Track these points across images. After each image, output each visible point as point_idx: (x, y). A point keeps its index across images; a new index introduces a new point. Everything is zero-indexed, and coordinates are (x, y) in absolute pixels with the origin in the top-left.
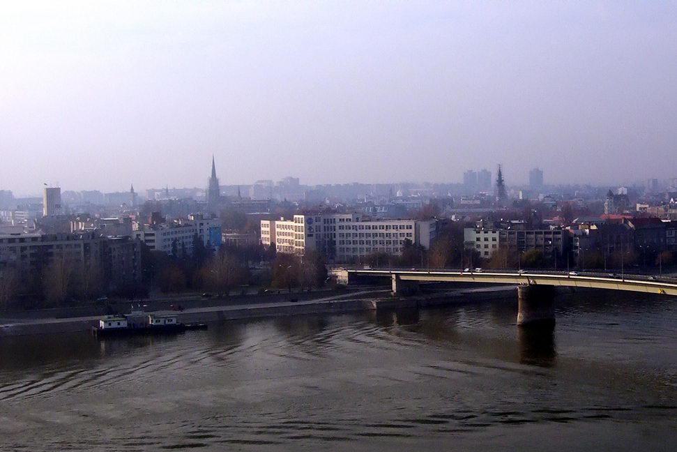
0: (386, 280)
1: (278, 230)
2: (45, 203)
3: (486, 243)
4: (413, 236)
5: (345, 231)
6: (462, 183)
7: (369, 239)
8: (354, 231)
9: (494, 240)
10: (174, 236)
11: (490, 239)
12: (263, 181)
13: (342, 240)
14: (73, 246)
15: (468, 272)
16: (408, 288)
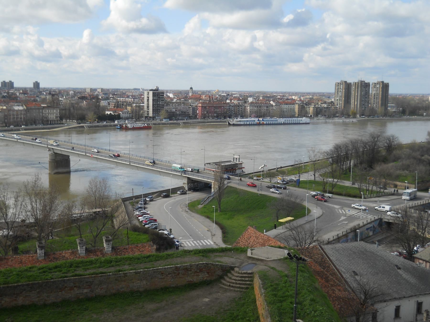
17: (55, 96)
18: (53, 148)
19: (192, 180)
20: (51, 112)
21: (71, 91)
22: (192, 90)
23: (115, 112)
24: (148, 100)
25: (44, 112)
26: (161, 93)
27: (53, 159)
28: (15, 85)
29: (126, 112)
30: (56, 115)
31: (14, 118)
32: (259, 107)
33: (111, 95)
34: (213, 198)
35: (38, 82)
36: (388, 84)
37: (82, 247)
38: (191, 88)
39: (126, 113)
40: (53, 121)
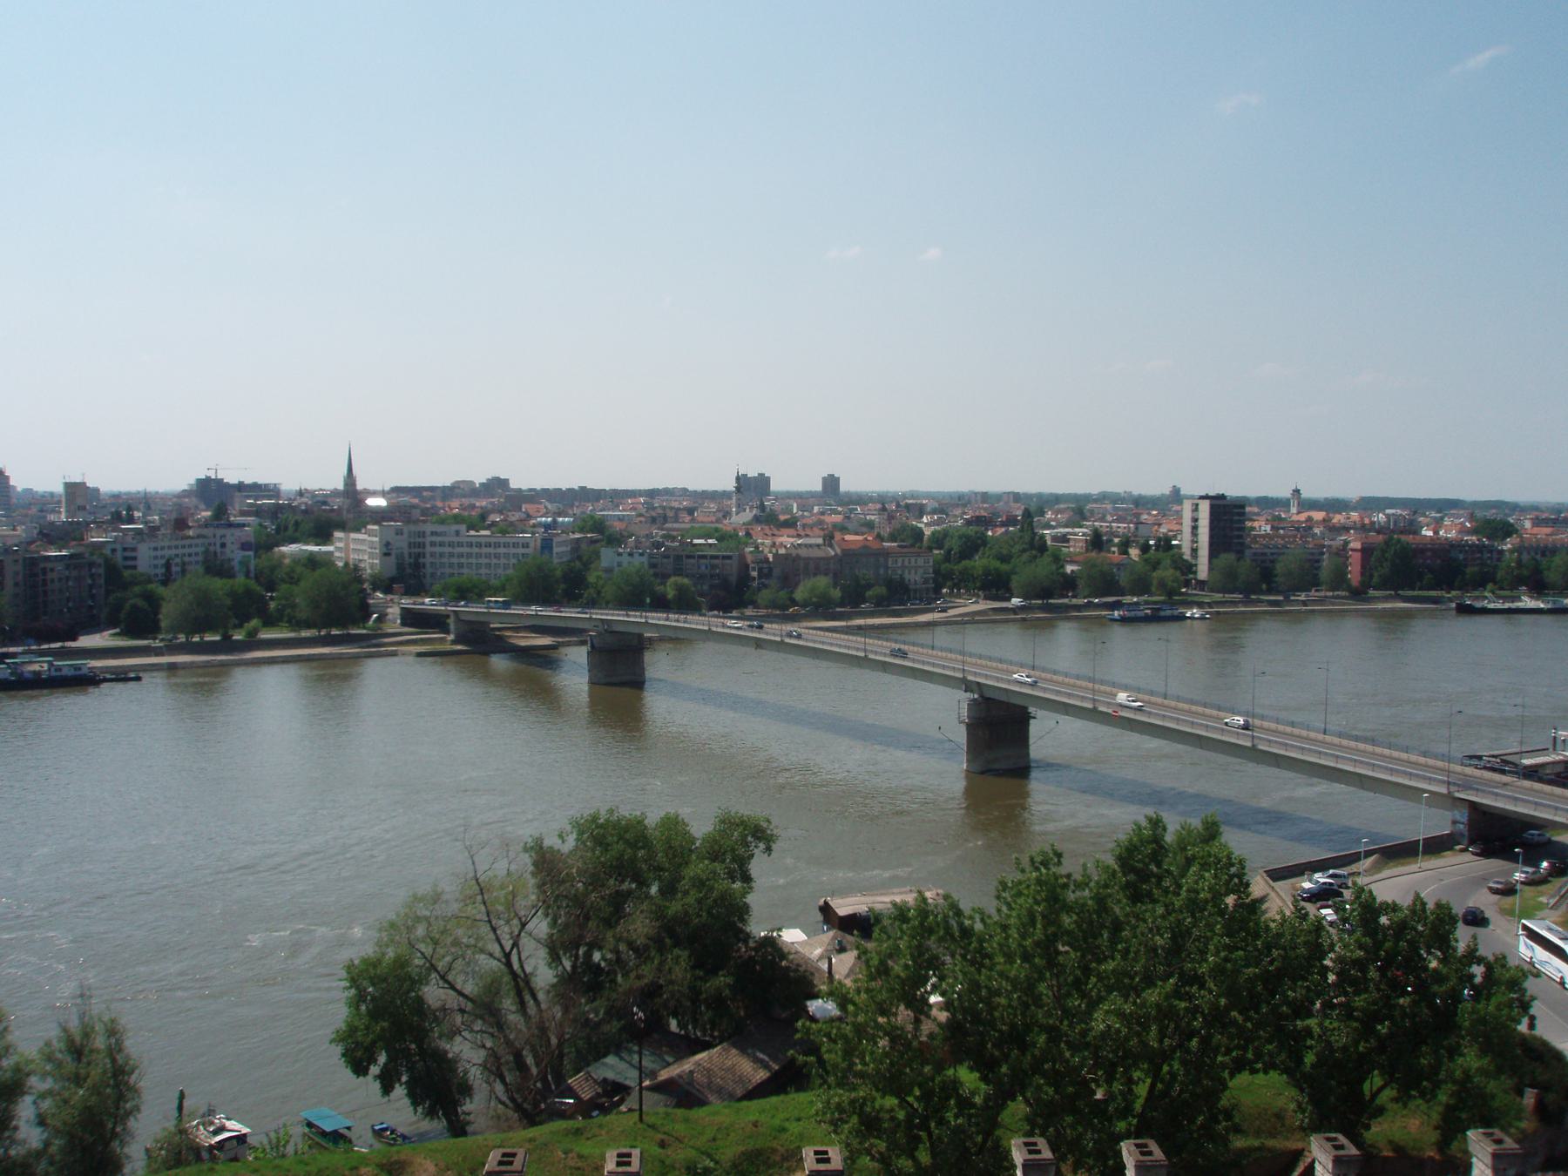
2: (63, 500)
5: (438, 549)
7: (462, 560)
8: (450, 550)
10: (167, 553)
14: (438, 555)
18: (978, 683)
19: (1485, 813)
22: (1299, 498)
24: (1195, 528)
25: (890, 565)
28: (775, 486)
30: (925, 573)
37: (1505, 1170)
38: (1297, 492)
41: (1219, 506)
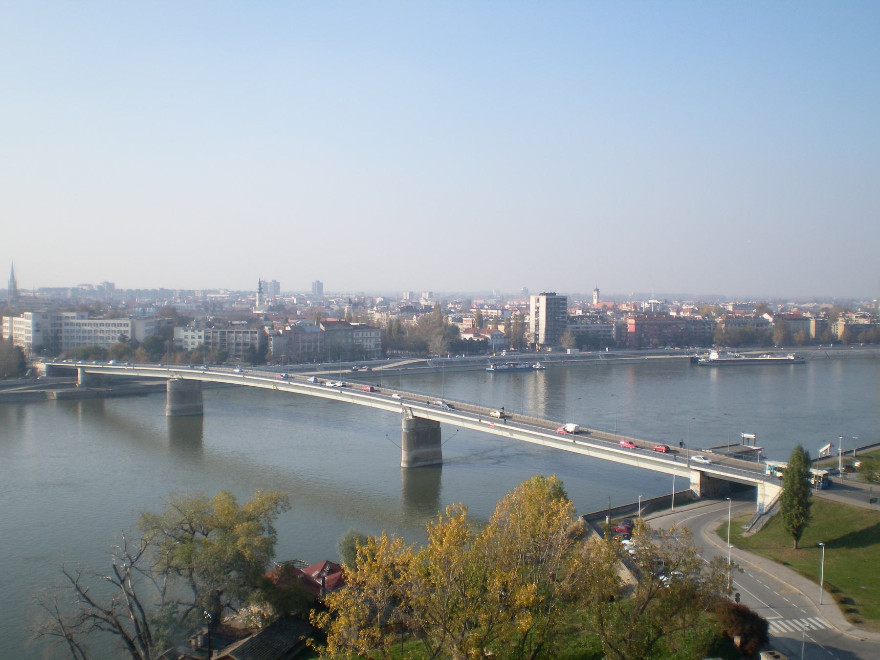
0: (73, 372)
1: (15, 326)
3: (193, 340)
4: (130, 332)
5: (70, 328)
6: (7, 289)
9: (200, 337)
11: (197, 337)
12: (83, 285)
13: (67, 335)
15: (81, 364)
16: (93, 380)
17: (359, 307)
20: (367, 335)
21: (378, 297)
23: (479, 336)
24: (537, 313)
25: (355, 336)
26: (561, 299)
27: (411, 429)
29: (499, 335)
30: (375, 341)
31: (303, 347)
32: (742, 325)
33: (450, 304)
34: (772, 518)
35: (321, 282)
36: (279, 283)
39: (499, 337)
40: (370, 352)
41: (551, 299)
